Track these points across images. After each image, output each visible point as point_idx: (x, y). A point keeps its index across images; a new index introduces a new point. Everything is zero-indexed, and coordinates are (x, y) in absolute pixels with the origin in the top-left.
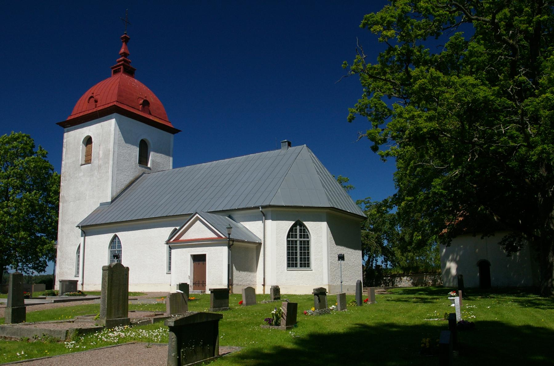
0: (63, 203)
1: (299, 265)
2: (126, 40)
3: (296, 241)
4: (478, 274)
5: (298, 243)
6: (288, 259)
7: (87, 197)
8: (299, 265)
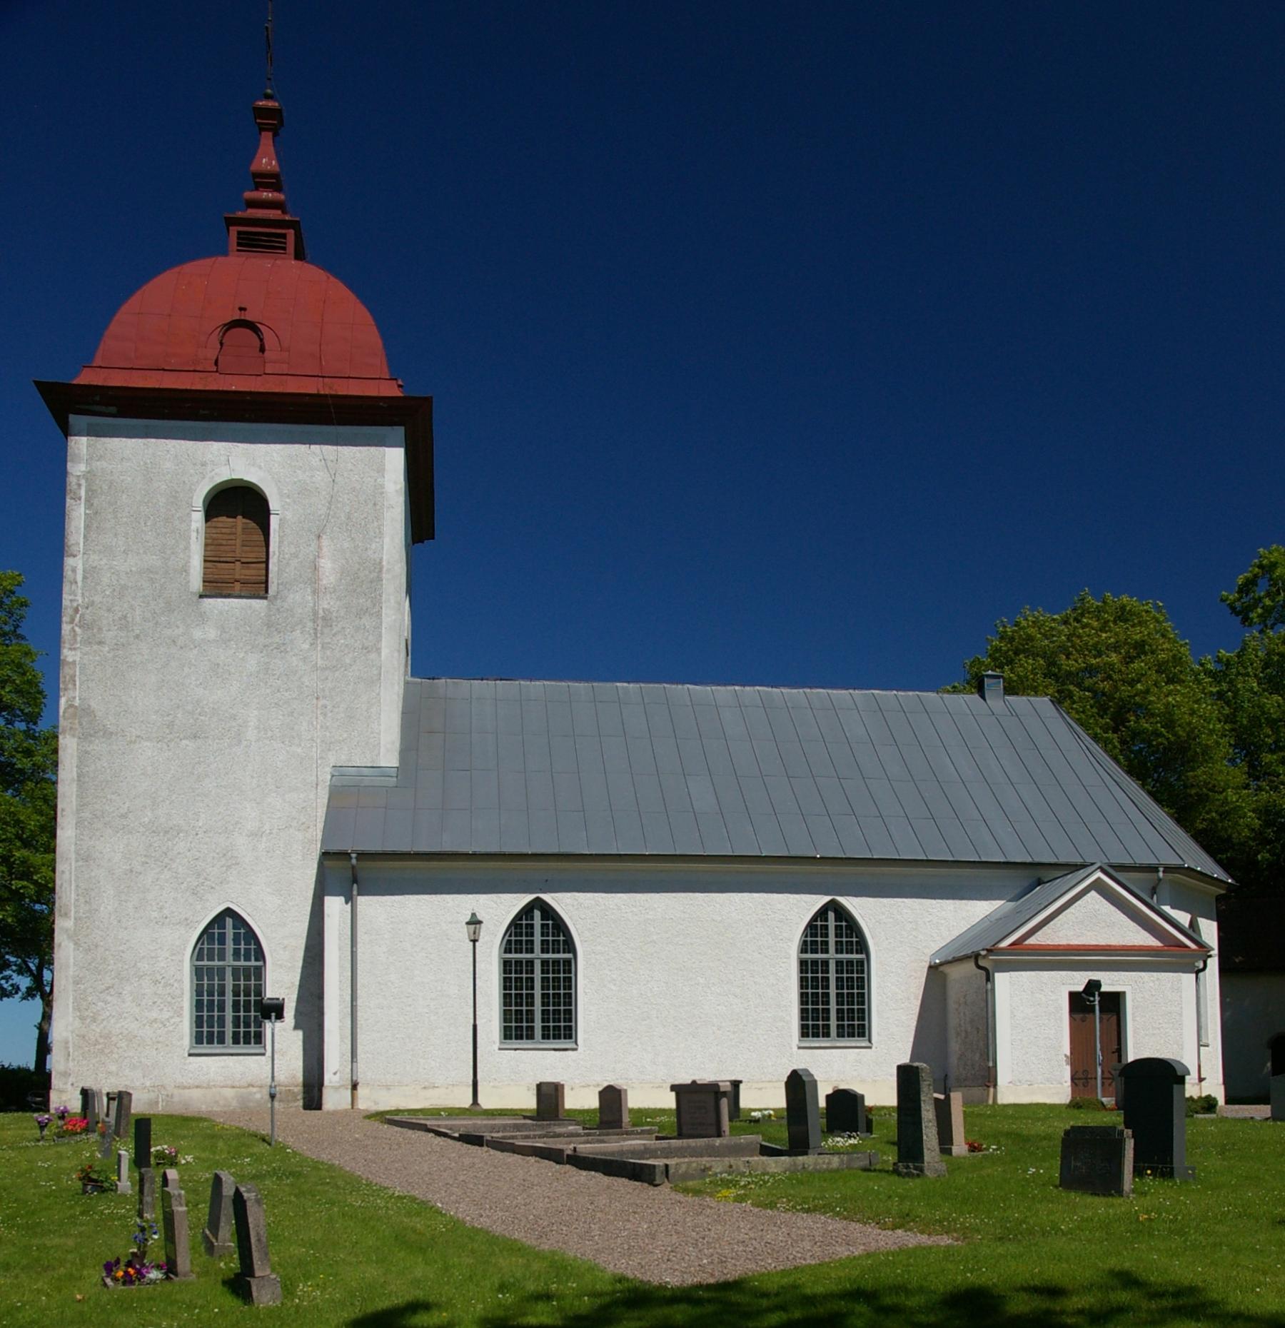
0: (85, 737)
1: (833, 1031)
2: (271, 121)
3: (530, 963)
4: (1269, 1064)
5: (832, 967)
6: (804, 1014)
7: (251, 734)
8: (833, 1031)
